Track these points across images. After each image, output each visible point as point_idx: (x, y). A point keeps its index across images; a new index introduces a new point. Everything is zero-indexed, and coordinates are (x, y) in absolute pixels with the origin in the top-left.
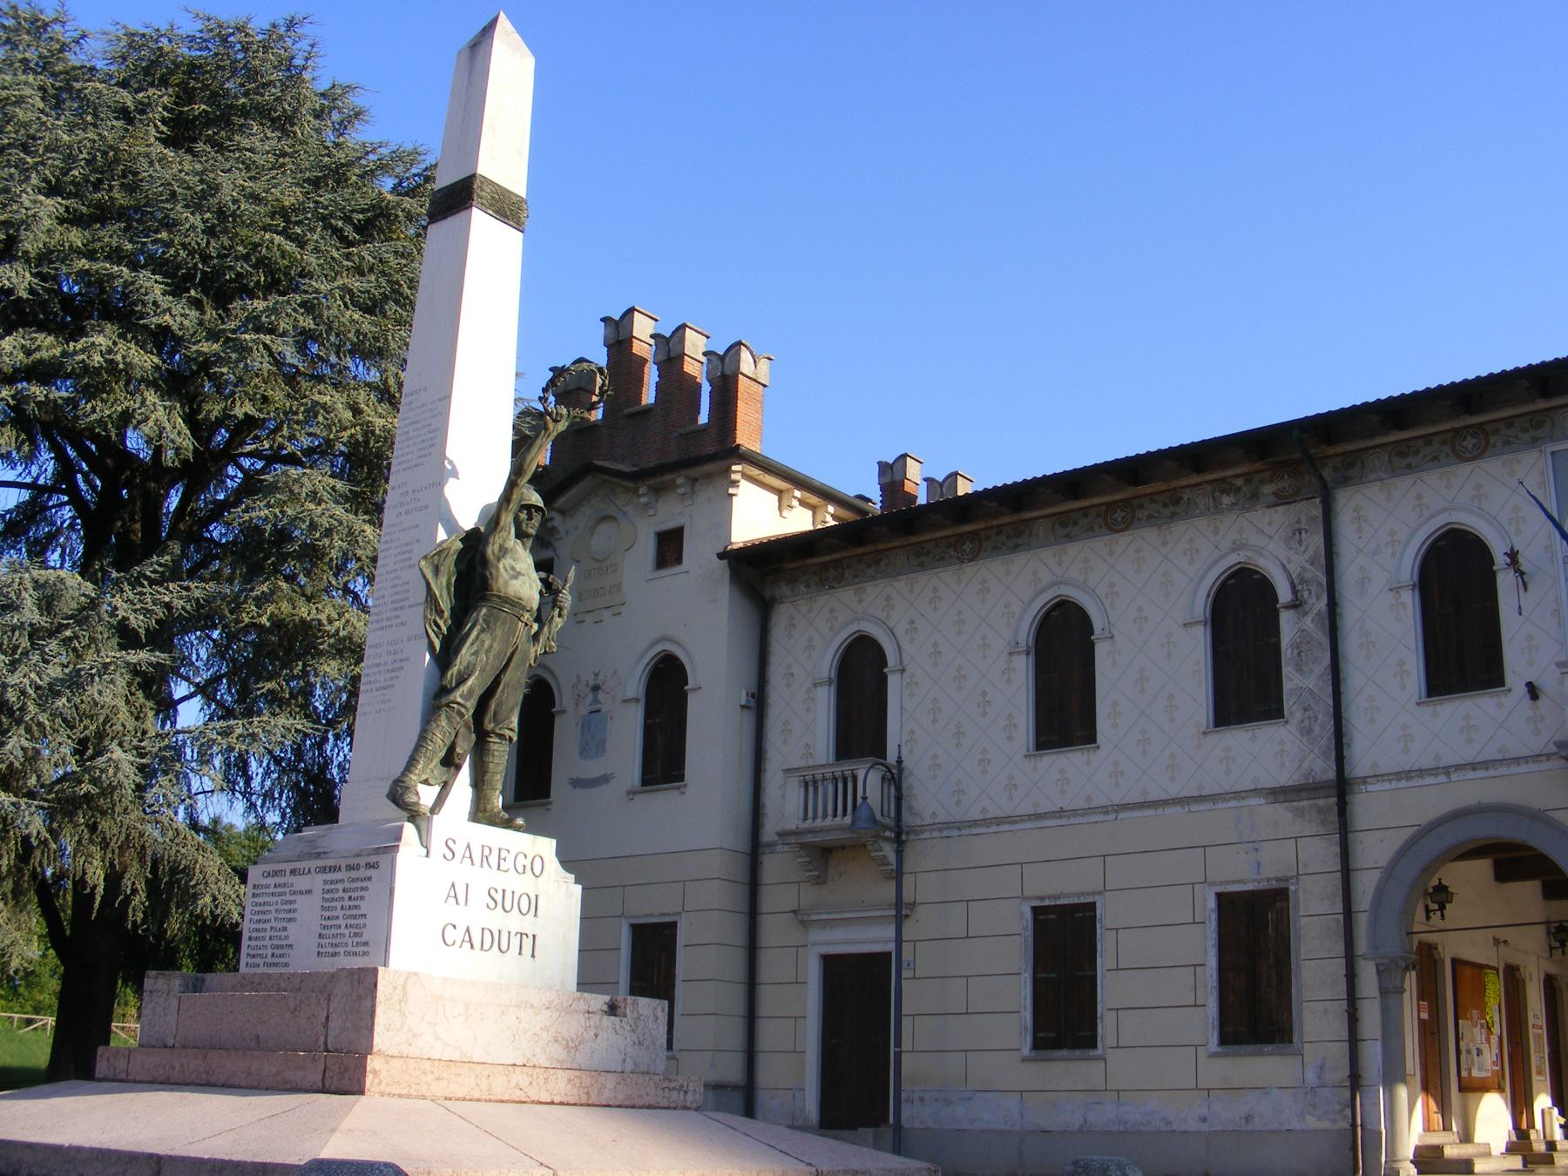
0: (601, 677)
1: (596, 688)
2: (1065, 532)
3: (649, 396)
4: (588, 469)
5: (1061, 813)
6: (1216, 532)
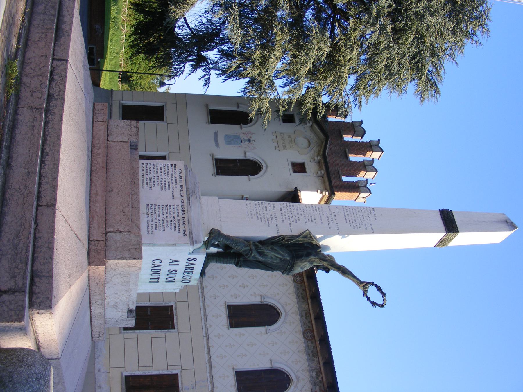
0: (254, 143)
1: (249, 140)
2: (304, 315)
3: (353, 158)
4: (327, 137)
5: (206, 316)
6: (303, 370)
